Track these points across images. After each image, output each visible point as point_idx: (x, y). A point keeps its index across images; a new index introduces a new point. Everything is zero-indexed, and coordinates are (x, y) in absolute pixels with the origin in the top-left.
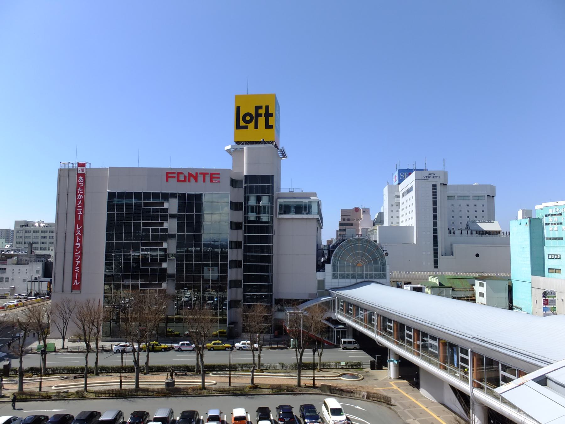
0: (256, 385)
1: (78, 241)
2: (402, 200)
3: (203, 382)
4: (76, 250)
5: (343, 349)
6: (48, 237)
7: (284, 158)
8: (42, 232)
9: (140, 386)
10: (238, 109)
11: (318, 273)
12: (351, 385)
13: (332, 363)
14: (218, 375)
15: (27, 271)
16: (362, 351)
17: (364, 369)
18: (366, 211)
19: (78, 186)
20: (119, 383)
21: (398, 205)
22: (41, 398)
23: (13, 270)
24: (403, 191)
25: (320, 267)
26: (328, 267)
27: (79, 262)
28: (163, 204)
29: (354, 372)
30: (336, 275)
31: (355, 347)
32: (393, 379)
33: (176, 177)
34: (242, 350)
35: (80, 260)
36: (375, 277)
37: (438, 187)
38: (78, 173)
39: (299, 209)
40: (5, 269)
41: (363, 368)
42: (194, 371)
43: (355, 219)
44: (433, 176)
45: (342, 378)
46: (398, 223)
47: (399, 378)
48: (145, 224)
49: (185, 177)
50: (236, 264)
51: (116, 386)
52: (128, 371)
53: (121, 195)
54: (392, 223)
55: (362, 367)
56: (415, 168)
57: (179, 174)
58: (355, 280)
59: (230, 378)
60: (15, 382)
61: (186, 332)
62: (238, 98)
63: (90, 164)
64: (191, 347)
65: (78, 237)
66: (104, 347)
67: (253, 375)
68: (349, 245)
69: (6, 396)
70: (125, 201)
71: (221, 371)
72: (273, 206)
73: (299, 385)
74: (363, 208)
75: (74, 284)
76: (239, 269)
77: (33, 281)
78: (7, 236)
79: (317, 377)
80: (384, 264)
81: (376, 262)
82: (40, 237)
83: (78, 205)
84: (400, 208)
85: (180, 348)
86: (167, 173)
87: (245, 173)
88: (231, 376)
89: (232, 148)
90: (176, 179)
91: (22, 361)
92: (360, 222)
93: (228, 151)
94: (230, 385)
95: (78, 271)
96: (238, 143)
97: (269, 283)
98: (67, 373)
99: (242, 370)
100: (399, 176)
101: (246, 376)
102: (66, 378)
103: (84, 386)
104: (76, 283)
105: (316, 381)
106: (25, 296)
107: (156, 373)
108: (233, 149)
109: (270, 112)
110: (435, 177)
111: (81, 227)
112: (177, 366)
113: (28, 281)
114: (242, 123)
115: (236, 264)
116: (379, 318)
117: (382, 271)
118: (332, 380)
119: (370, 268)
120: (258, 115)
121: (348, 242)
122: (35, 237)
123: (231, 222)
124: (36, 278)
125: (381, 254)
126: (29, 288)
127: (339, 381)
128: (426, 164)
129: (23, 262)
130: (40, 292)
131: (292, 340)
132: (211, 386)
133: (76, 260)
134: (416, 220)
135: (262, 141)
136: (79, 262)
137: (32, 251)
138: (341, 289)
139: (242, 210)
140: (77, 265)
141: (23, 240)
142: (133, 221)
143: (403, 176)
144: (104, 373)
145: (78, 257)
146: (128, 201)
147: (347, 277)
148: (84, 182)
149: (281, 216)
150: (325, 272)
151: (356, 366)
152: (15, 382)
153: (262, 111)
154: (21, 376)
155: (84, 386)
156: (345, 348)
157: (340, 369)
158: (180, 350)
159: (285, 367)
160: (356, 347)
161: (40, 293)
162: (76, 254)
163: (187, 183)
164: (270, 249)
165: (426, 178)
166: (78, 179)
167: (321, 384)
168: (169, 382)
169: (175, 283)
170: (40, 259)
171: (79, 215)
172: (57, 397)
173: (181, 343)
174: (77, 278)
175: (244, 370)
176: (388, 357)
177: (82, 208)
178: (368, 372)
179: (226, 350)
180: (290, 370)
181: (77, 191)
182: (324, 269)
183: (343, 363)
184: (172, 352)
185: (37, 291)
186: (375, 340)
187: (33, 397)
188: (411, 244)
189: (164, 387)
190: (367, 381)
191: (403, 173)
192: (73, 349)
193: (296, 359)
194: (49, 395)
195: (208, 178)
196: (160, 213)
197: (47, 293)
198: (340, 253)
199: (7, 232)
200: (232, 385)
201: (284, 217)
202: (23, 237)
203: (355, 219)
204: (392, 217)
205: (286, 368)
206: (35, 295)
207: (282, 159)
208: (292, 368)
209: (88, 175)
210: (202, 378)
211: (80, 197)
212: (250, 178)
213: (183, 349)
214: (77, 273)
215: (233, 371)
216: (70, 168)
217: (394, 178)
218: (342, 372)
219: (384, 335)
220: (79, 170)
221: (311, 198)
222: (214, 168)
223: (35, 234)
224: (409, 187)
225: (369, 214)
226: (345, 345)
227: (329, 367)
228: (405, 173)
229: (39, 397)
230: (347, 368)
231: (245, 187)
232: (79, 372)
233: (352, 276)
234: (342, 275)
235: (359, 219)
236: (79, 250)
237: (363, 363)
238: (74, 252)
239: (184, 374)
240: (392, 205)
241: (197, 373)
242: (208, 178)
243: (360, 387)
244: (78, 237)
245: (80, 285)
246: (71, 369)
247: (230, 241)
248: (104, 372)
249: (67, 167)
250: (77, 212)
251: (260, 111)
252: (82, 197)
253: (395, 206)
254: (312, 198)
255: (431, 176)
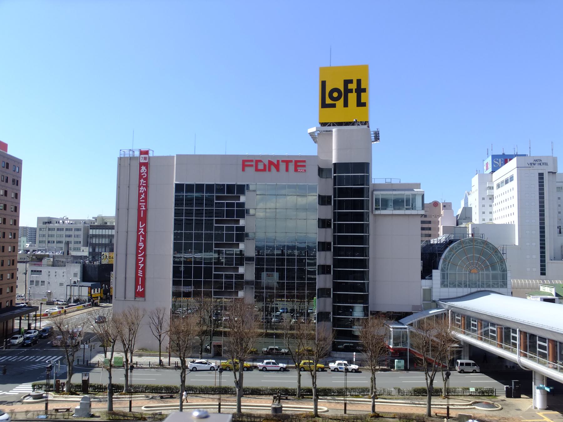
0: (378, 413)
1: (141, 241)
2: (496, 192)
3: (316, 409)
4: (139, 251)
5: (460, 372)
6: (73, 236)
7: (376, 142)
8: (67, 229)
9: (242, 411)
10: (323, 84)
11: (424, 281)
12: (491, 415)
13: (458, 388)
14: (326, 401)
15: (65, 274)
16: (483, 374)
17: (497, 396)
18: (447, 206)
19: (141, 177)
20: (218, 407)
21: (492, 198)
22: (135, 419)
23: (49, 272)
24: (499, 181)
25: (426, 273)
26: (436, 273)
27: (143, 265)
28: (238, 198)
29: (485, 400)
30: (446, 283)
31: (474, 370)
32: (540, 409)
33: (254, 166)
34: (338, 371)
35: (144, 262)
36: (494, 286)
37: (546, 176)
38: (141, 161)
39: (398, 203)
40: (41, 271)
41: (496, 396)
42: (295, 395)
43: (433, 216)
44: (539, 162)
45: (476, 407)
46: (491, 220)
47: (547, 409)
48: (217, 222)
49: (265, 165)
50: (325, 270)
51: (212, 409)
52: (218, 392)
53: (190, 188)
54: (484, 220)
55: (494, 394)
56: (517, 153)
57: (257, 162)
58: (469, 289)
59: (345, 404)
60: (98, 400)
61: (265, 349)
62: (322, 70)
63: (153, 151)
64: (278, 366)
65: (141, 236)
66: (177, 364)
67: (374, 402)
68: (461, 246)
69: (96, 415)
70: (195, 194)
71: (327, 395)
72: (369, 200)
73: (429, 415)
74: (443, 202)
75: (137, 291)
76: (328, 276)
77: (72, 286)
78: (24, 234)
79: (452, 405)
80: (504, 270)
81: (494, 268)
82: (64, 236)
83: (141, 199)
84: (493, 202)
85: (264, 367)
86: (244, 161)
87: (334, 161)
88: (347, 402)
89: (317, 131)
90: (253, 168)
91: (111, 377)
92: (440, 219)
93: (312, 134)
94: (345, 413)
95: (142, 276)
96: (323, 124)
97: (364, 292)
98: (150, 392)
99: (351, 395)
100: (493, 163)
101: (356, 402)
102: (152, 398)
103: (179, 407)
104: (140, 289)
105: (450, 410)
106: (64, 303)
107: (251, 396)
108: (319, 132)
109: (362, 87)
110: (542, 164)
111: (144, 224)
112: (274, 388)
113: (67, 286)
114: (328, 101)
115: (325, 270)
116: (522, 335)
117: (501, 278)
118: (464, 409)
119: (488, 276)
120: (348, 91)
121: (460, 244)
122: (60, 236)
123: (319, 219)
124: (75, 282)
125: (501, 258)
126: (68, 294)
127: (474, 411)
128: (530, 148)
129: (59, 264)
130: (80, 298)
131: (397, 360)
132: (323, 413)
133: (139, 263)
134: (518, 217)
135: (354, 122)
136: (143, 265)
137: (68, 252)
138: (454, 300)
139: (331, 204)
140: (140, 269)
141: (47, 239)
142: (204, 218)
143: (495, 162)
144: (192, 394)
145: (142, 259)
146: (199, 195)
147: (459, 286)
148: (147, 173)
149: (377, 212)
150: (431, 279)
151: (487, 393)
152: (98, 400)
153: (353, 86)
154: (111, 394)
155: (179, 407)
156: (462, 371)
157: (468, 396)
158: (265, 370)
159: (402, 393)
160: (475, 370)
161: (80, 299)
162: (139, 255)
163: (267, 173)
164: (364, 252)
165: (531, 165)
166: (140, 169)
167: (459, 414)
168: (277, 408)
169: (254, 291)
170: (77, 261)
171: (142, 211)
172: (153, 419)
173: (265, 361)
174: (140, 284)
175: (353, 395)
176: (533, 383)
177: (146, 202)
178: (504, 400)
179: (319, 371)
180: (408, 396)
181: (140, 182)
182: (431, 276)
183: (472, 390)
184: (255, 372)
185: (77, 297)
186: (517, 364)
187: (126, 418)
188: (512, 245)
189: (270, 412)
190: (508, 412)
191: (498, 159)
192: (142, 365)
193: (426, 384)
194: (144, 416)
195: (292, 166)
196: (235, 209)
197: (87, 300)
198: (450, 256)
199: (24, 230)
200: (347, 412)
201: (381, 214)
202: (47, 236)
203: (433, 216)
204: (484, 213)
205: (403, 394)
206: (75, 301)
207: (373, 143)
208: (410, 394)
209: (152, 164)
210: (315, 404)
211: (142, 189)
212: (338, 167)
213: (268, 368)
214: (140, 278)
215: (341, 396)
216: (131, 156)
217: (486, 165)
218: (473, 400)
219: (531, 357)
220: (141, 158)
221: (414, 191)
222: (299, 154)
223: (59, 233)
224: (508, 176)
225: (451, 209)
226: (462, 367)
227: (455, 393)
228: (500, 160)
229: (133, 418)
230: (476, 395)
231: (335, 177)
232: (163, 392)
233: (466, 284)
234: (453, 283)
235: (438, 216)
236: (142, 251)
237: (495, 389)
238: (137, 253)
239: (285, 398)
240: (483, 199)
241: (299, 397)
242: (292, 166)
243: (503, 418)
244: (141, 236)
245: (144, 292)
246: (154, 387)
247: (318, 242)
248: (191, 392)
249: (127, 156)
250: (139, 207)
251: (350, 86)
252: (145, 190)
253: (487, 199)
254: (415, 190)
255: (537, 162)
